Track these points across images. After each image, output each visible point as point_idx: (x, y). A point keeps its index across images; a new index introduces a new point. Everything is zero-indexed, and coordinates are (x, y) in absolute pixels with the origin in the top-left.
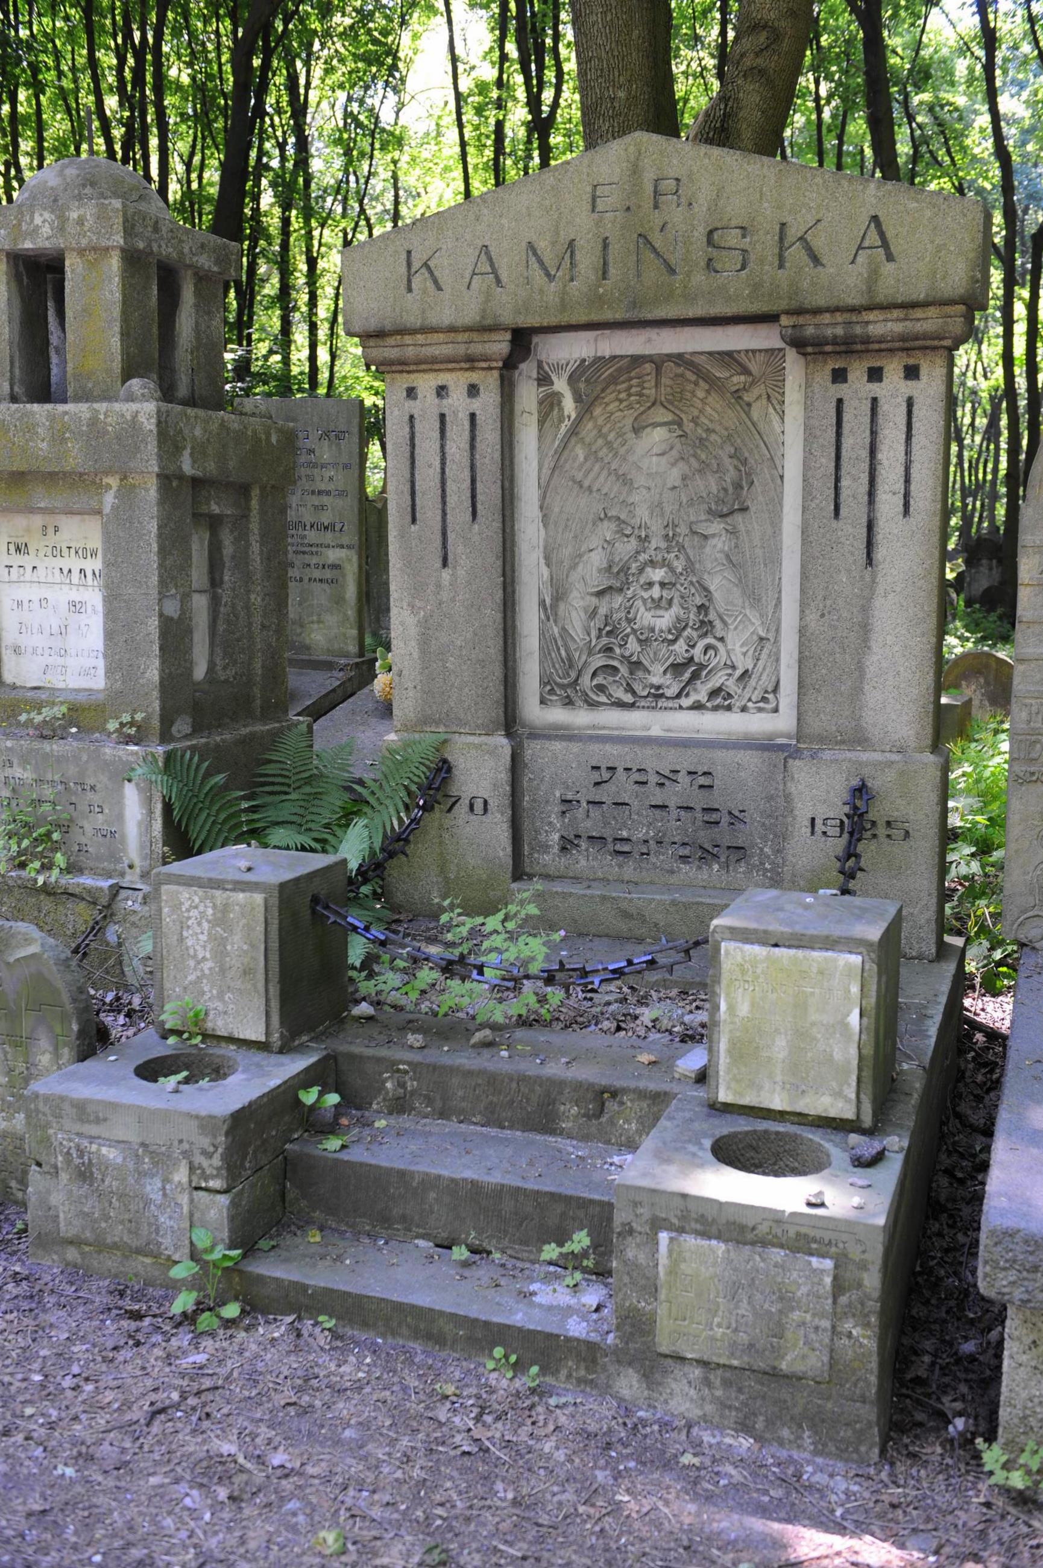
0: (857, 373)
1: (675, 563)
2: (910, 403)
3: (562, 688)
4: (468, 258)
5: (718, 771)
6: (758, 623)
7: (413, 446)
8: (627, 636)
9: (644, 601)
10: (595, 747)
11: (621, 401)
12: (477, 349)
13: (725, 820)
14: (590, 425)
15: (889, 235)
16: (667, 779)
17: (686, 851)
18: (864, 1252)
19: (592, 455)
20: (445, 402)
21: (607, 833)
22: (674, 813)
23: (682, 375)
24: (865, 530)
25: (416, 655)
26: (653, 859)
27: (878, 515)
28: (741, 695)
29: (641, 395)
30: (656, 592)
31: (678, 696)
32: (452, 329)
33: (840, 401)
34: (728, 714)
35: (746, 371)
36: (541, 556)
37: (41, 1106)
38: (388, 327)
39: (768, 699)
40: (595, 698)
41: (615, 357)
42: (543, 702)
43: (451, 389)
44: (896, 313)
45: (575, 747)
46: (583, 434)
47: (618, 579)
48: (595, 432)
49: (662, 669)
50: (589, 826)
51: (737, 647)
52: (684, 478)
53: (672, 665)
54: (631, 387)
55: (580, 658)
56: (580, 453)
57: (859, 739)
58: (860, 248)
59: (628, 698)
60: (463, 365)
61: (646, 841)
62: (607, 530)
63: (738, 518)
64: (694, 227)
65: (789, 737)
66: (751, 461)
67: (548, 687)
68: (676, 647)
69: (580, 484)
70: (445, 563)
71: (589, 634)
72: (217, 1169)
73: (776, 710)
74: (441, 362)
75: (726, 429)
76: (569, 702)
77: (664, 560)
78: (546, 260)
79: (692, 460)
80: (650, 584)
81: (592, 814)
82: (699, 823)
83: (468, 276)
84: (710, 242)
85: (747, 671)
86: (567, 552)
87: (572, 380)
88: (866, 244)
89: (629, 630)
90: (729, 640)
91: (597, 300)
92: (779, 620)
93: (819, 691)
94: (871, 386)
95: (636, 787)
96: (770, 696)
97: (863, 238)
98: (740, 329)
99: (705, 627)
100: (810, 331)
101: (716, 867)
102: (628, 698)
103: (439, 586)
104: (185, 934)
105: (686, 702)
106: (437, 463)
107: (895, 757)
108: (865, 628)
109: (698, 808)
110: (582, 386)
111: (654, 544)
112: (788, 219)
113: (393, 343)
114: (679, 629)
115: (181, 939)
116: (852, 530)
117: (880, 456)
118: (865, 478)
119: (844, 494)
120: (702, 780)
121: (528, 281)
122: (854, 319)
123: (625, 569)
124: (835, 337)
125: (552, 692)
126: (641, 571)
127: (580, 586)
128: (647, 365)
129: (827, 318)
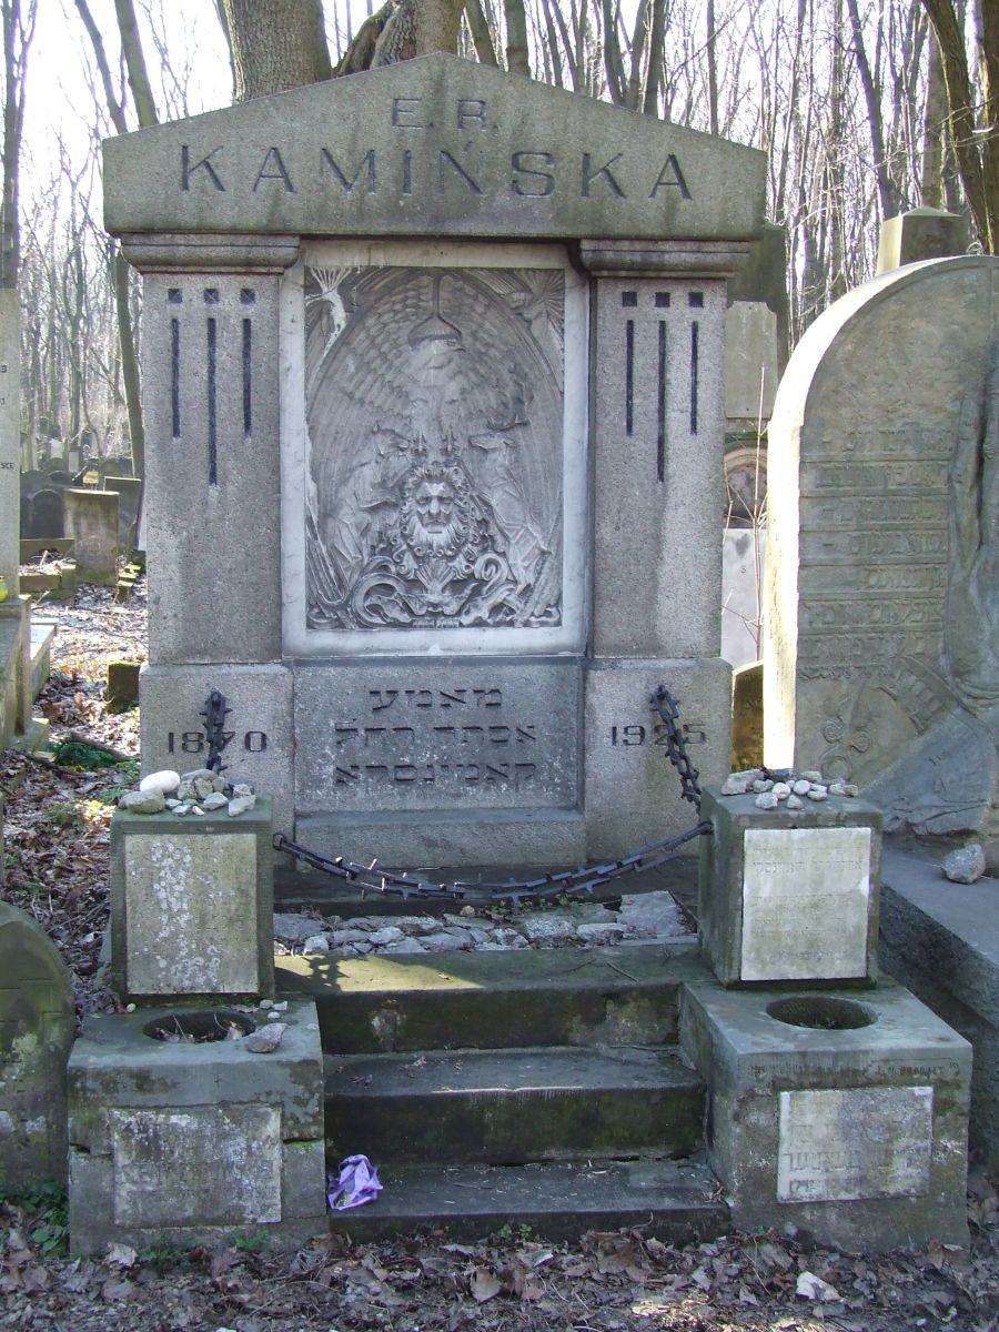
0: (646, 296)
1: (454, 478)
2: (695, 328)
3: (330, 608)
4: (255, 158)
5: (506, 687)
6: (539, 537)
7: (176, 352)
8: (403, 553)
9: (421, 516)
10: (374, 671)
11: (396, 312)
12: (259, 253)
13: (514, 736)
14: (362, 335)
15: (686, 172)
16: (452, 699)
17: (473, 773)
18: (957, 1073)
19: (364, 366)
20: (214, 306)
21: (389, 762)
22: (461, 733)
23: (461, 289)
24: (656, 445)
25: (177, 579)
26: (438, 784)
27: (668, 431)
28: (523, 610)
29: (417, 307)
30: (434, 507)
31: (459, 613)
32: (234, 231)
33: (630, 323)
34: (510, 630)
35: (528, 290)
36: (308, 469)
37: (90, 1084)
38: (159, 225)
39: (550, 613)
40: (369, 619)
41: (391, 267)
42: (310, 625)
43: (221, 292)
44: (689, 246)
45: (352, 672)
46: (355, 344)
47: (393, 494)
48: (367, 343)
49: (440, 587)
50: (365, 756)
51: (519, 561)
52: (463, 391)
53: (452, 581)
54: (407, 298)
55: (351, 578)
56: (351, 365)
57: (653, 648)
58: (659, 183)
59: (405, 618)
60: (239, 269)
61: (430, 766)
62: (382, 444)
63: (519, 432)
64: (500, 150)
65: (572, 650)
66: (531, 376)
67: (316, 610)
68: (455, 563)
69: (351, 396)
70: (213, 477)
71: (361, 553)
72: (314, 1116)
73: (558, 623)
74: (215, 265)
75: (506, 344)
76: (339, 625)
77: (442, 474)
78: (342, 167)
79: (471, 374)
80: (428, 500)
81: (371, 743)
82: (487, 742)
83: (253, 175)
84: (516, 165)
85: (529, 585)
86: (336, 467)
87: (343, 289)
88: (664, 180)
89: (405, 547)
90: (510, 554)
91: (396, 212)
92: (561, 533)
93: (614, 602)
94: (658, 310)
95: (419, 710)
96: (553, 610)
97: (662, 175)
98: (499, 250)
99: (487, 542)
100: (610, 256)
101: (504, 786)
102: (405, 618)
103: (205, 503)
104: (156, 886)
105: (466, 620)
106: (204, 371)
107: (689, 663)
108: (657, 540)
109: (485, 727)
110: (354, 295)
111: (432, 457)
112: (592, 150)
113: (161, 242)
114: (458, 543)
115: (150, 893)
116: (643, 446)
117: (668, 376)
118: (655, 396)
119: (636, 411)
120: (489, 699)
121: (323, 188)
122: (651, 247)
123: (401, 486)
124: (633, 263)
125: (321, 615)
126: (418, 485)
127: (351, 501)
128: (424, 278)
129: (625, 245)
